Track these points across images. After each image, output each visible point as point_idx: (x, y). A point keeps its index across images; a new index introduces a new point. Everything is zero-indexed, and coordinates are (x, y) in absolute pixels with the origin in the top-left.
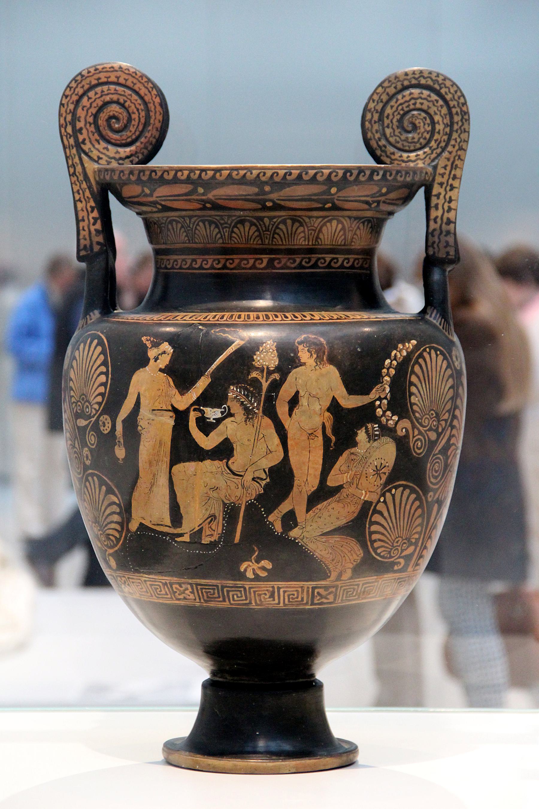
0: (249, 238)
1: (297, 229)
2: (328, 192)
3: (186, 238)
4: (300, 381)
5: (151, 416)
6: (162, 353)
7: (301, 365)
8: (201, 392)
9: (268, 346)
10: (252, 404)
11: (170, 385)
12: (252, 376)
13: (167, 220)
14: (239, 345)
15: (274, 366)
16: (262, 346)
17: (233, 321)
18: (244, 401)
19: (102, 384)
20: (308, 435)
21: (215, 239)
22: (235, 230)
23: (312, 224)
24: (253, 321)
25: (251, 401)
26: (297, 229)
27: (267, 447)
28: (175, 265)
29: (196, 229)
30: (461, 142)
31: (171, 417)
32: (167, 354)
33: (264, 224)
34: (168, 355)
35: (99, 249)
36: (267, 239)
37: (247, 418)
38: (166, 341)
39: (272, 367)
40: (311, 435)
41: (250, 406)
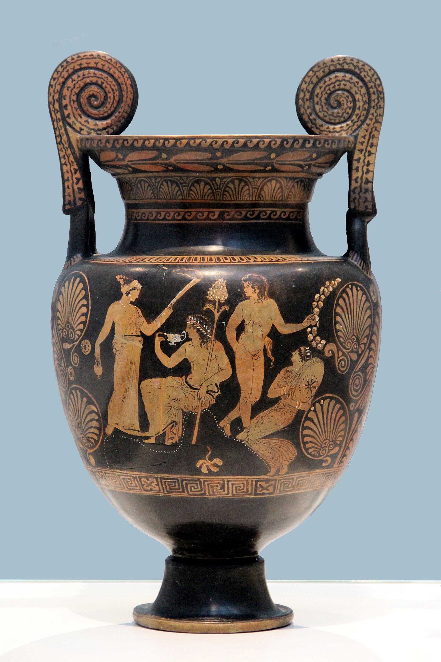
0: (204, 194)
1: (243, 188)
2: (268, 157)
3: (152, 195)
4: (246, 312)
5: (124, 341)
6: (133, 289)
7: (246, 299)
9: (219, 283)
10: (206, 331)
11: (139, 315)
12: (206, 308)
13: (136, 180)
15: (225, 300)
18: (200, 329)
19: (83, 314)
20: (252, 356)
21: (176, 196)
22: (193, 188)
23: (256, 183)
24: (207, 262)
25: (205, 328)
26: (243, 188)
27: (219, 366)
28: (143, 217)
29: (160, 187)
31: (140, 341)
32: (136, 290)
33: (216, 183)
34: (138, 290)
36: (218, 195)
37: (202, 342)
38: (136, 279)
39: (223, 300)
40: (255, 356)
41: (204, 333)
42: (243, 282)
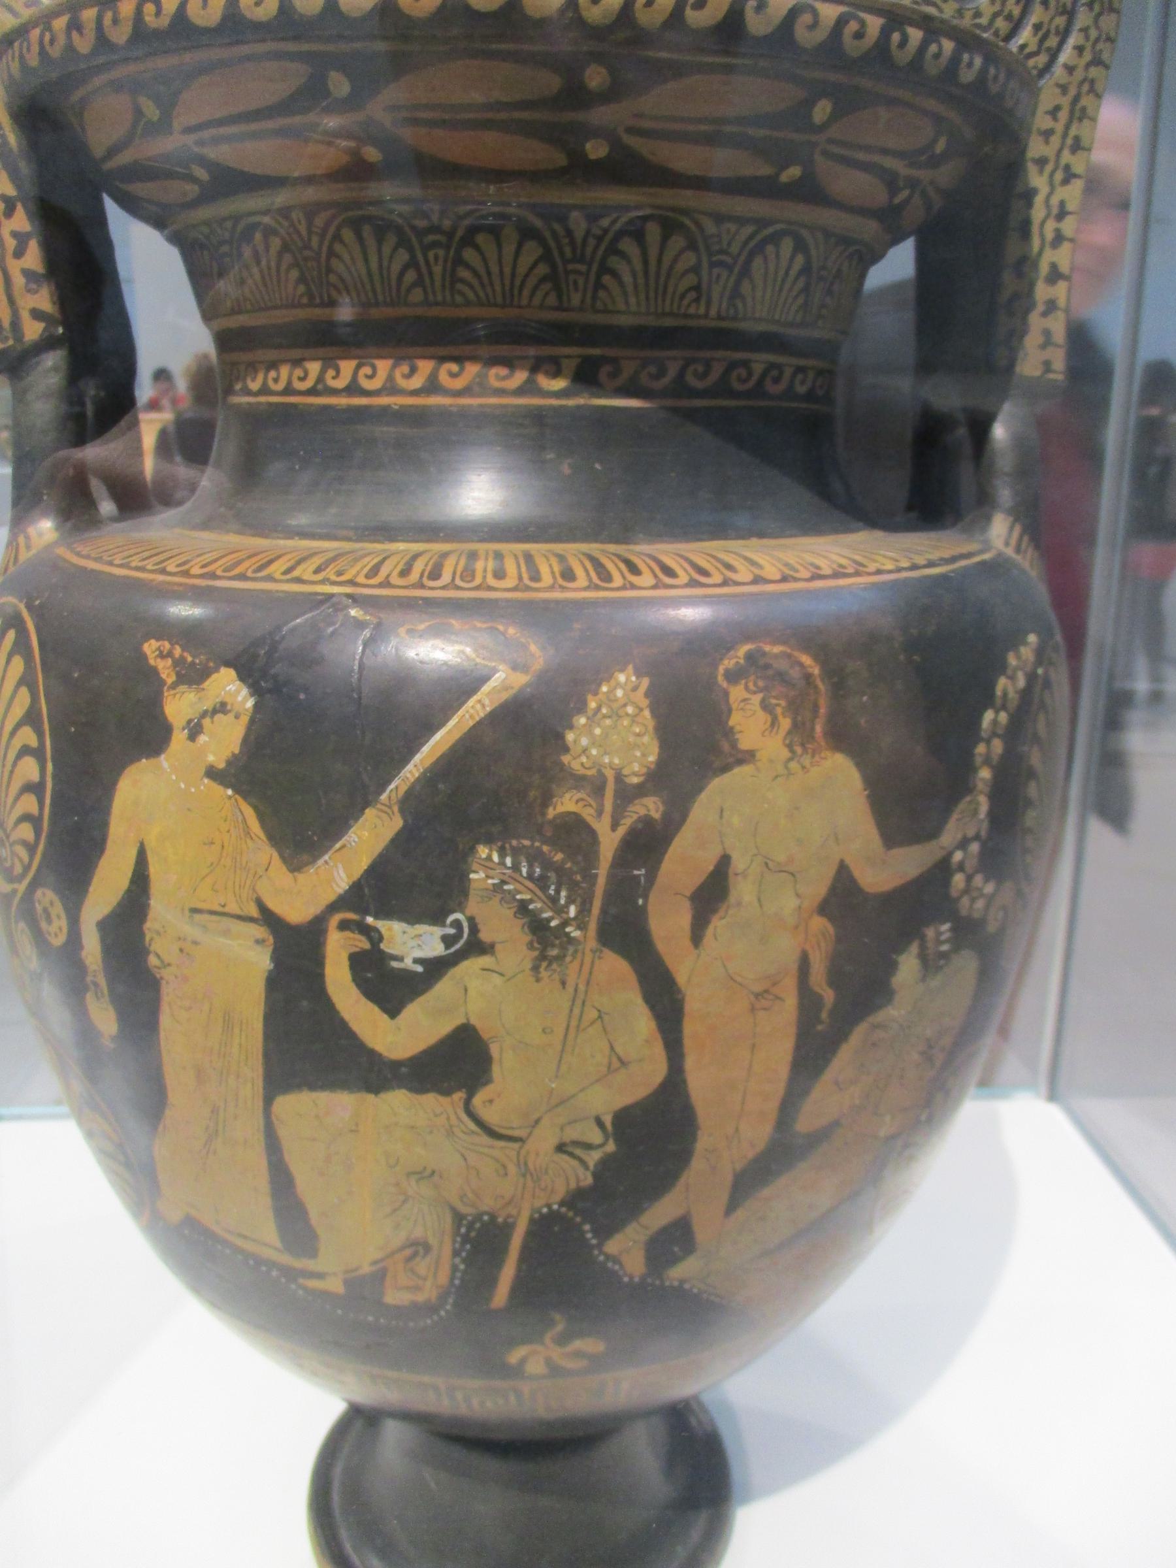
0: (518, 282)
1: (675, 260)
2: (799, 115)
3: (302, 289)
4: (736, 821)
5: (190, 931)
6: (215, 712)
7: (740, 762)
8: (364, 863)
9: (619, 693)
10: (561, 910)
11: (248, 832)
12: (561, 809)
13: (234, 226)
14: (506, 689)
15: (644, 770)
16: (596, 693)
17: (478, 588)
18: (531, 901)
19: (29, 788)
20: (752, 998)
21: (398, 290)
22: (469, 254)
23: (725, 243)
24: (551, 588)
25: (554, 900)
26: (675, 260)
27: (612, 1048)
28: (271, 383)
29: (331, 253)
30: (1097, 40)
31: (258, 942)
32: (231, 716)
33: (569, 233)
34: (237, 717)
35: (40, 331)
36: (576, 289)
37: (543, 957)
38: (228, 664)
39: (635, 771)
40: (764, 996)
41: (552, 918)
42: (725, 685)
